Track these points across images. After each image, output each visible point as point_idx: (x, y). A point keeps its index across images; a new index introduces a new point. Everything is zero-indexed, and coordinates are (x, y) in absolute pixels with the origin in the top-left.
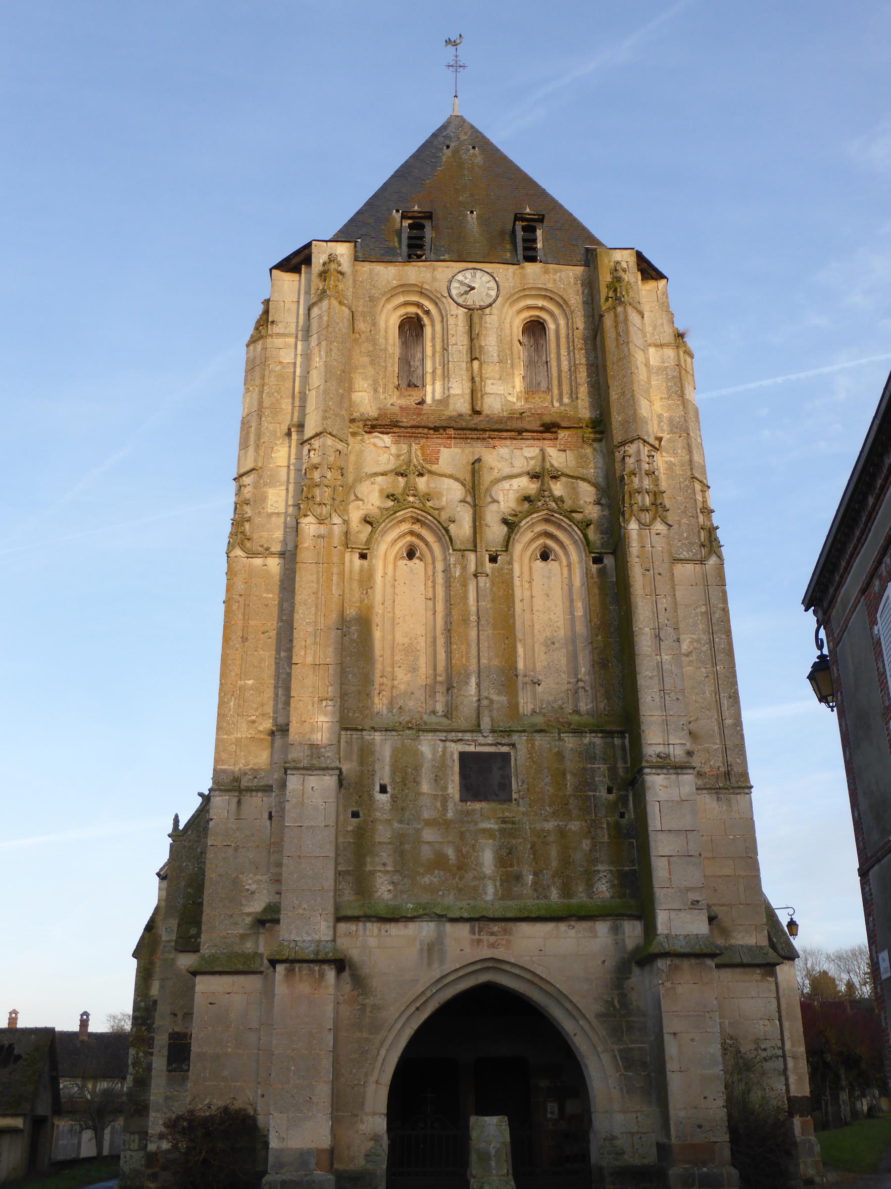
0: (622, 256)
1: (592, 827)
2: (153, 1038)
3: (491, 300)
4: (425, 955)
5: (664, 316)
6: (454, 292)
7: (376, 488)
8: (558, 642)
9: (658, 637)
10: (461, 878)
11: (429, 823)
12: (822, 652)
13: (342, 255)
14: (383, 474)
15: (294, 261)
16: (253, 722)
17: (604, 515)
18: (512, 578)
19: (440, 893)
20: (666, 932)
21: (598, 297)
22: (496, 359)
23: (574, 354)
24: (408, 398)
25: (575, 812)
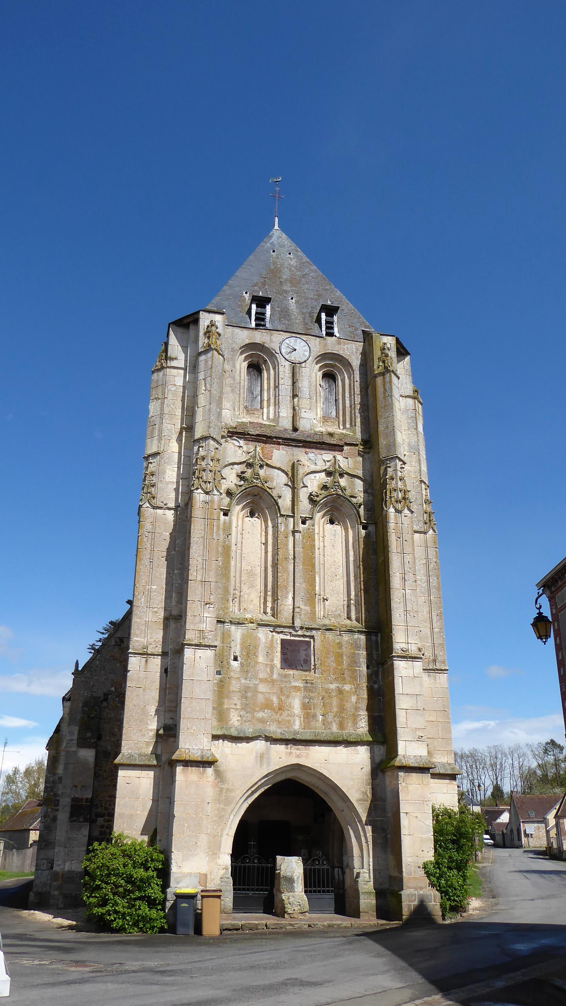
0: (388, 340)
1: (357, 688)
2: (58, 801)
3: (306, 359)
4: (259, 760)
5: (407, 378)
6: (283, 351)
7: (234, 471)
8: (339, 575)
9: (404, 579)
10: (281, 715)
11: (262, 680)
12: (539, 611)
13: (218, 322)
14: (240, 463)
15: (186, 321)
16: (156, 612)
17: (369, 500)
18: (314, 535)
19: (268, 723)
20: (403, 754)
21: (371, 364)
22: (308, 396)
23: (354, 397)
24: (252, 415)
25: (348, 679)
